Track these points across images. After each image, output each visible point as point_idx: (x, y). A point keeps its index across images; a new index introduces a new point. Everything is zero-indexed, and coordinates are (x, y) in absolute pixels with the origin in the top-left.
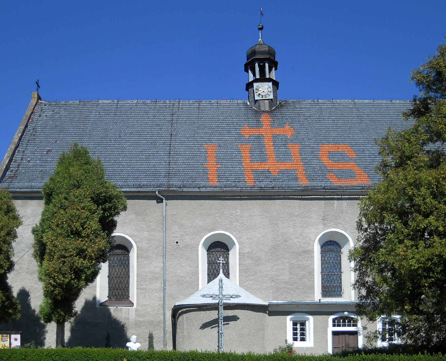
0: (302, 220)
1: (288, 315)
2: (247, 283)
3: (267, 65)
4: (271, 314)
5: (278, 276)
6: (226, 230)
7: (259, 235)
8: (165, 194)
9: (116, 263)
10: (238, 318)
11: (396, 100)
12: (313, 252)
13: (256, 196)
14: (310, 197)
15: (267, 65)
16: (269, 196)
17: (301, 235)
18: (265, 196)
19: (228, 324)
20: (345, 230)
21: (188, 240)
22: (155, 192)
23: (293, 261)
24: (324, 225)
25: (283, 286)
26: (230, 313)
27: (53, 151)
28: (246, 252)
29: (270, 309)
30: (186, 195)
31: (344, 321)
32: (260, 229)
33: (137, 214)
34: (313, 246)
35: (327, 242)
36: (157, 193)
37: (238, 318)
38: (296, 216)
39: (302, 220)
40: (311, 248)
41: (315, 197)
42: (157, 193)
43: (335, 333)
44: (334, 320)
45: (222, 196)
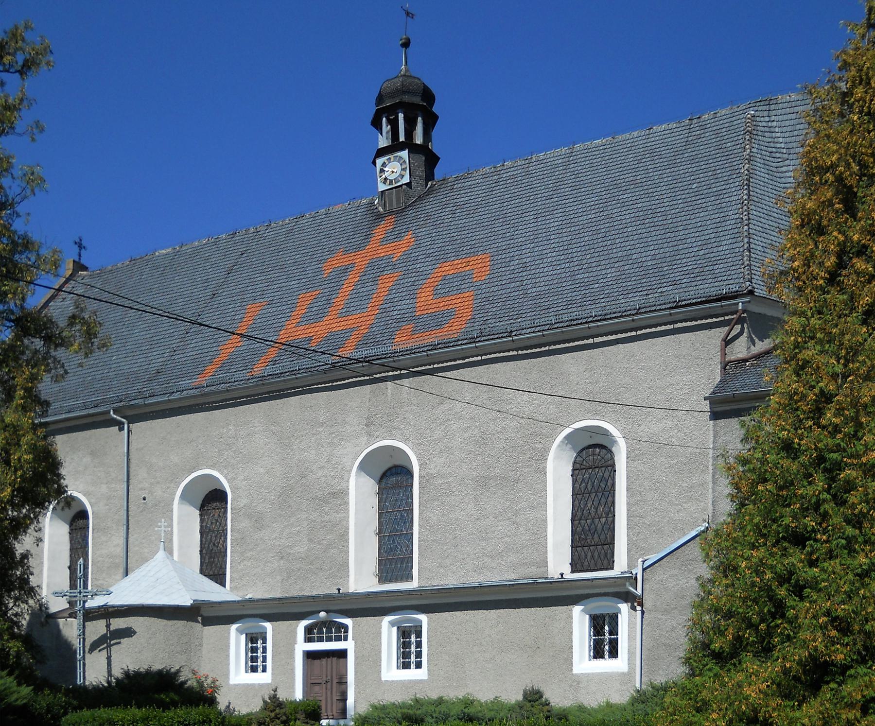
0: (332, 430)
1: (233, 623)
2: (242, 564)
3: (401, 116)
4: (208, 621)
5: (290, 547)
6: (212, 467)
7: (262, 470)
8: (130, 413)
9: (79, 542)
10: (135, 633)
11: (661, 124)
12: (347, 494)
13: (259, 394)
14: (347, 381)
15: (401, 116)
16: (279, 391)
17: (328, 461)
18: (273, 392)
19: (120, 643)
20: (406, 441)
21: (158, 492)
22: (109, 412)
23: (314, 515)
24: (369, 434)
25: (298, 566)
26: (118, 623)
27: (786, 210)
28: (242, 505)
29: (206, 612)
30: (157, 409)
31: (329, 631)
32: (264, 459)
33: (93, 454)
34: (348, 481)
35: (390, 469)
36: (112, 413)
37: (135, 633)
38: (322, 425)
39: (332, 430)
40: (344, 485)
41: (354, 379)
42: (112, 413)
43: (310, 656)
44: (306, 628)
45: (208, 403)
